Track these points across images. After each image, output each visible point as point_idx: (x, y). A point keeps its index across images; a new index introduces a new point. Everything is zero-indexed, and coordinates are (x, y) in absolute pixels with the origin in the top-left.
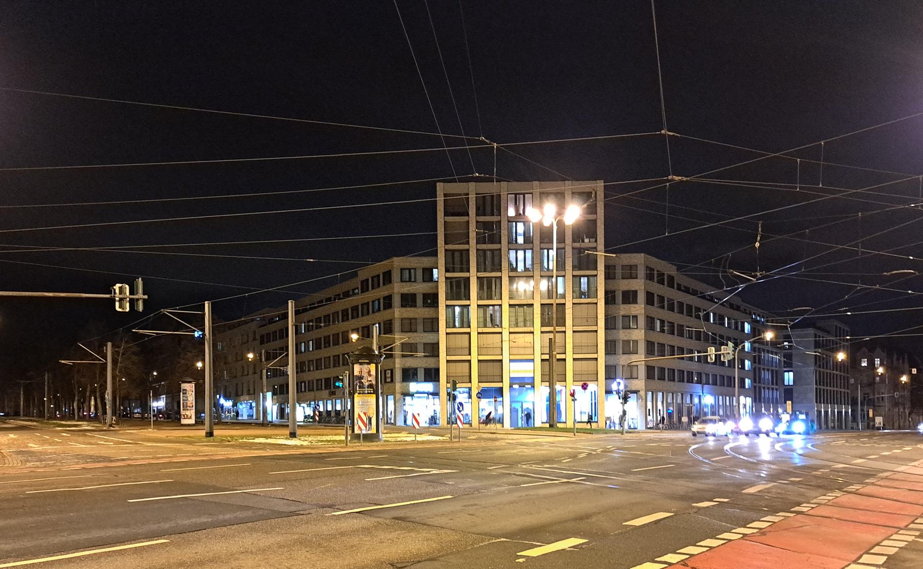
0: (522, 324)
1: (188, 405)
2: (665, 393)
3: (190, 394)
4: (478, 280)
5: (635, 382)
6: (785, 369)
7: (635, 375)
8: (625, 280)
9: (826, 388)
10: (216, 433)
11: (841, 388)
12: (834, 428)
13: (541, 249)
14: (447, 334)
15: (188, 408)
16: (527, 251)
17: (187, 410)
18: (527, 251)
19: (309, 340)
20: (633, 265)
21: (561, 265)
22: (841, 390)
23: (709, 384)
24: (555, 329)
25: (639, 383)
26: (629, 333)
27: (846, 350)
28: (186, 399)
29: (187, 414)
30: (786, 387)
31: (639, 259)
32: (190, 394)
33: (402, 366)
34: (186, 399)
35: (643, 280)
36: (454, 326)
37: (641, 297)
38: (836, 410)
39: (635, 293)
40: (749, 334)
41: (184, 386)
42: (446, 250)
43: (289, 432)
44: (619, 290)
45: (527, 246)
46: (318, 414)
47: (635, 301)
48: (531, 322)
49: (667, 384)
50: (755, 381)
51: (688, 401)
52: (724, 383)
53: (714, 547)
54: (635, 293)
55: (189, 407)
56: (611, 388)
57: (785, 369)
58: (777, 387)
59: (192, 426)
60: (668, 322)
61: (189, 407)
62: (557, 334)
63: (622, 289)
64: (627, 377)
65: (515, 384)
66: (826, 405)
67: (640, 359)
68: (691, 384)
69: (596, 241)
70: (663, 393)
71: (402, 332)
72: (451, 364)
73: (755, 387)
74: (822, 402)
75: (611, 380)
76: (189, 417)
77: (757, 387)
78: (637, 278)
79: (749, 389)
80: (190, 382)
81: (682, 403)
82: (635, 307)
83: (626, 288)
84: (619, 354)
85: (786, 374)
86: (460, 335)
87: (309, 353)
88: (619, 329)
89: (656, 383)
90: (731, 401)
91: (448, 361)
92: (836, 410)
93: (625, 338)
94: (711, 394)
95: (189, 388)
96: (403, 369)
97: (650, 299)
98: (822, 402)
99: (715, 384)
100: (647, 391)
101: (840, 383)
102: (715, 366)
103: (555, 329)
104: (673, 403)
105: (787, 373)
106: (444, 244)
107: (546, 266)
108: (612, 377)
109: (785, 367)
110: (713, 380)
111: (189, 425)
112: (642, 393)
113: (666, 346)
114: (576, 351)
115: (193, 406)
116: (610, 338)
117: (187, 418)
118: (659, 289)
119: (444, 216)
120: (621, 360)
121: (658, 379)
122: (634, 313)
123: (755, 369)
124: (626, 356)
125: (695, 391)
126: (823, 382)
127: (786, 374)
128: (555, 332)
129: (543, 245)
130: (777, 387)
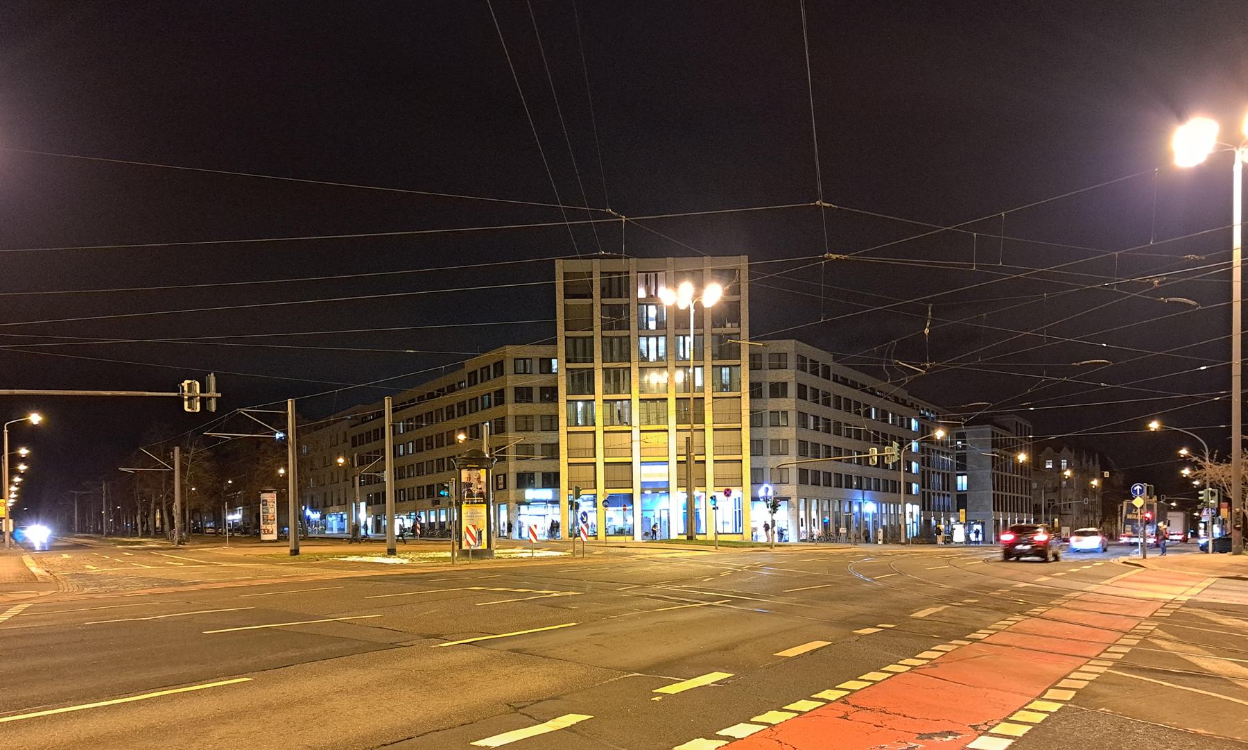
0: (655, 421)
2: (820, 501)
5: (785, 487)
10: (302, 550)
16: (659, 338)
25: (790, 489)
30: (958, 493)
36: (577, 425)
37: (792, 390)
41: (264, 496)
47: (785, 395)
49: (821, 489)
50: (923, 487)
55: (270, 520)
61: (270, 520)
67: (790, 460)
70: (818, 500)
80: (271, 492)
83: (775, 380)
85: (959, 478)
89: (809, 489)
90: (896, 509)
91: (569, 464)
93: (774, 437)
97: (802, 392)
108: (759, 481)
109: (957, 470)
111: (270, 541)
112: (794, 500)
118: (811, 381)
120: (769, 462)
121: (812, 484)
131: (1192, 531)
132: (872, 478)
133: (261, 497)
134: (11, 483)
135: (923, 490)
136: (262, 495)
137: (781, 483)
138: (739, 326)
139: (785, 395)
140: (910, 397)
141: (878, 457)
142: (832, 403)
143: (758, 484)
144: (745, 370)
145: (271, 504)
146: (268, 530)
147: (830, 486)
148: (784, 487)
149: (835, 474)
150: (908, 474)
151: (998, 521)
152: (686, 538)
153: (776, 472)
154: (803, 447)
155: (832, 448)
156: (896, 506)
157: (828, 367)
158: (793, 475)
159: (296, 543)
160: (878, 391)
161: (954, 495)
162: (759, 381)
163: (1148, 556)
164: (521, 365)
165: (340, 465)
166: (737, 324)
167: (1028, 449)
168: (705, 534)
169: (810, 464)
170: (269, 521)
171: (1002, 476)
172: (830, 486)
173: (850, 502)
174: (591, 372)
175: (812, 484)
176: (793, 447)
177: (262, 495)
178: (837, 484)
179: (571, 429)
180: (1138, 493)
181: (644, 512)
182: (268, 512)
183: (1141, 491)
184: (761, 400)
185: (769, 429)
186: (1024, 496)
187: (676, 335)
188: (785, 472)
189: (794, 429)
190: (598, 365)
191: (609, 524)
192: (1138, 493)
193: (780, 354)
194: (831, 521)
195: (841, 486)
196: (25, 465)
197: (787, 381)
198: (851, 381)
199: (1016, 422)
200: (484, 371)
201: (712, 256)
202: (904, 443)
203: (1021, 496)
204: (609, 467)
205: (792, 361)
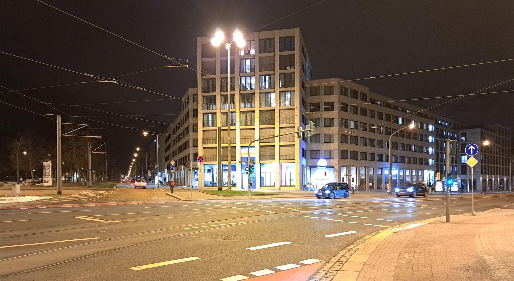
0: (244, 124)
4: (223, 97)
5: (332, 160)
6: (462, 154)
9: (490, 165)
10: (63, 192)
11: (497, 164)
12: (371, 188)
13: (260, 75)
14: (204, 131)
15: (46, 176)
18: (247, 78)
21: (271, 85)
23: (397, 162)
25: (335, 162)
26: (328, 129)
28: (45, 171)
29: (46, 180)
30: (463, 165)
31: (335, 82)
33: (193, 152)
34: (45, 171)
36: (209, 126)
37: (337, 106)
38: (499, 179)
39: (333, 103)
40: (432, 131)
41: (45, 164)
43: (56, 191)
45: (252, 74)
47: (333, 109)
49: (368, 163)
50: (437, 161)
51: (379, 173)
53: (257, 276)
54: (333, 103)
55: (47, 176)
56: (317, 164)
57: (462, 154)
59: (49, 187)
61: (47, 176)
63: (324, 101)
64: (353, 158)
65: (244, 162)
66: (496, 176)
67: (335, 146)
68: (381, 162)
69: (295, 68)
70: (356, 167)
71: (194, 132)
72: (206, 149)
73: (438, 164)
74: (498, 173)
75: (317, 160)
76: (47, 182)
77: (498, 167)
79: (432, 165)
80: (47, 161)
81: (374, 174)
82: (332, 113)
83: (327, 101)
84: (322, 143)
85: (463, 157)
89: (349, 161)
90: (417, 173)
91: (204, 148)
92: (499, 179)
93: (326, 133)
94: (396, 168)
95: (47, 165)
96: (194, 154)
97: (344, 108)
98: (498, 173)
99: (403, 162)
102: (403, 151)
106: (201, 75)
107: (264, 85)
109: (461, 152)
111: (48, 186)
112: (337, 168)
113: (359, 138)
115: (49, 175)
117: (46, 182)
118: (350, 101)
119: (201, 58)
120: (323, 146)
122: (332, 117)
123: (437, 153)
124: (327, 144)
126: (494, 161)
127: (463, 157)
129: (261, 73)
131: (334, 191)
132: (399, 156)
133: (43, 164)
134: (157, 167)
136: (43, 163)
137: (330, 158)
139: (333, 109)
141: (303, 132)
142: (465, 132)
143: (317, 159)
146: (46, 181)
147: (366, 160)
148: (331, 160)
149: (419, 158)
150: (427, 154)
154: (344, 139)
156: (417, 171)
159: (59, 188)
163: (452, 218)
165: (138, 151)
166: (293, 67)
167: (490, 138)
169: (350, 147)
170: (46, 176)
172: (366, 160)
174: (215, 96)
176: (337, 138)
177: (43, 163)
178: (402, 161)
180: (472, 153)
181: (243, 174)
182: (45, 172)
183: (475, 151)
184: (319, 112)
185: (324, 128)
186: (493, 165)
187: (260, 75)
188: (332, 152)
190: (218, 94)
192: (472, 153)
196: (26, 152)
200: (329, 124)
203: (499, 166)
205: (337, 90)
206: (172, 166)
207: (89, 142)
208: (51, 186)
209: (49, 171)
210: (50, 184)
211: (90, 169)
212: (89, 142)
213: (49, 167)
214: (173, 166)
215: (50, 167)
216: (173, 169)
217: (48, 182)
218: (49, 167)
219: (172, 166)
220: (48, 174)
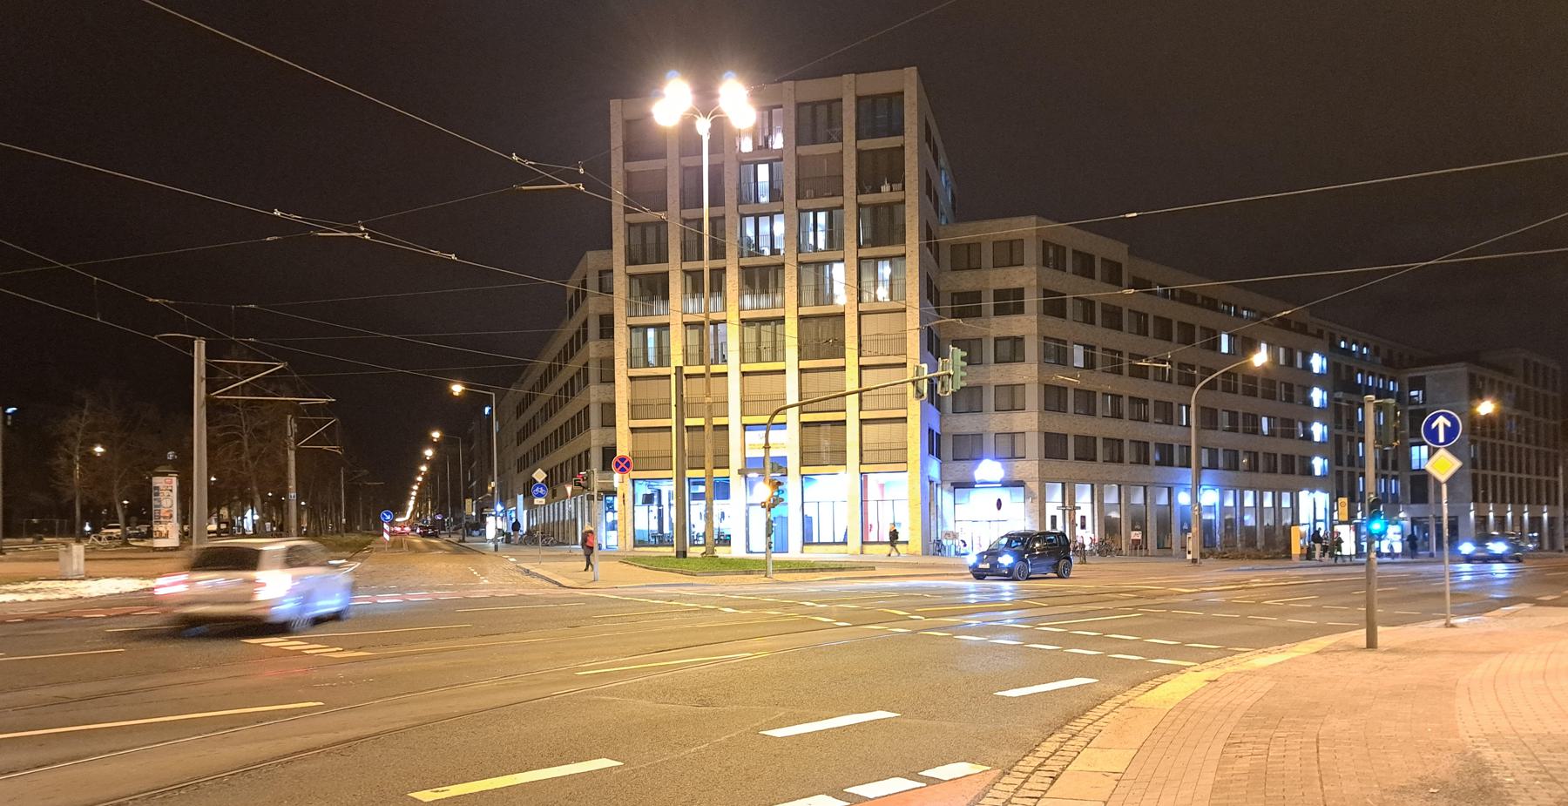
0: (754, 357)
1: (162, 515)
2: (1095, 486)
3: (166, 494)
4: (689, 278)
5: (1019, 464)
7: (1018, 453)
8: (1000, 270)
13: (743, 216)
15: (162, 519)
16: (775, 216)
17: (160, 523)
19: (1181, 402)
20: (1016, 240)
22: (1521, 476)
24: (708, 369)
25: (1028, 468)
27: (1497, 392)
28: (158, 504)
29: (160, 529)
30: (1415, 473)
31: (1026, 228)
32: (166, 494)
35: (1034, 268)
36: (647, 365)
37: (1032, 300)
38: (1526, 516)
41: (158, 481)
42: (859, 206)
44: (988, 289)
45: (776, 206)
46: (385, 534)
47: (1019, 309)
48: (777, 352)
49: (1127, 471)
50: (1339, 462)
52: (1293, 468)
55: (164, 517)
56: (973, 477)
58: (1395, 473)
60: (1104, 350)
61: (164, 517)
62: (712, 379)
67: (1028, 421)
68: (1167, 468)
70: (1092, 485)
71: (602, 382)
76: (163, 535)
78: (1022, 265)
79: (1323, 477)
80: (165, 474)
81: (1145, 503)
83: (1002, 285)
85: (1415, 450)
86: (644, 382)
87: (1179, 428)
88: (988, 364)
89: (1071, 467)
90: (1277, 501)
91: (633, 430)
93: (1001, 381)
94: (1214, 487)
95: (164, 484)
96: (603, 448)
97: (1054, 306)
100: (1043, 481)
101: (1538, 462)
102: (1233, 434)
103: (708, 369)
104: (1120, 503)
105: (1417, 448)
108: (976, 457)
109: (1411, 437)
110: (1181, 457)
111: (166, 549)
112: (1034, 486)
114: (976, 408)
115: (171, 516)
116: (607, 387)
118: (1071, 285)
121: (1076, 459)
124: (1001, 415)
125: (1180, 481)
128: (708, 375)
129: (803, 204)
130: (1395, 473)
133: (153, 481)
135: (1339, 468)
138: (903, 189)
140: (1313, 319)
141: (930, 380)
144: (912, 263)
145: (166, 493)
148: (1017, 464)
150: (1306, 442)
151: (1486, 518)
152: (674, 554)
153: (1006, 440)
154: (1054, 398)
155: (1151, 403)
157: (1119, 266)
158: (1033, 445)
160: (1224, 304)
161: (1407, 476)
162: (978, 288)
164: (1005, 348)
168: (845, 543)
169: (1072, 424)
170: (162, 519)
171: (1493, 445)
173: (1169, 489)
175: (1076, 459)
176: (1033, 397)
178: (1269, 467)
179: (635, 372)
180: (1442, 439)
183: (1451, 433)
186: (1508, 475)
187: (800, 211)
189: (1035, 367)
191: (693, 529)
192: (1442, 439)
193: (1011, 241)
194: (1123, 520)
195: (1275, 471)
196: (102, 447)
197: (1024, 285)
198: (1296, 323)
199: (1526, 362)
201: (856, 73)
202: (1198, 379)
204: (694, 433)
205: (1031, 253)
206: (537, 486)
207: (290, 416)
208: (176, 549)
209: (169, 504)
210: (173, 541)
211: (292, 495)
212: (290, 416)
213: (171, 491)
214: (540, 486)
215: (175, 490)
216: (540, 495)
217: (167, 536)
218: (171, 491)
219: (537, 486)
220: (168, 511)
